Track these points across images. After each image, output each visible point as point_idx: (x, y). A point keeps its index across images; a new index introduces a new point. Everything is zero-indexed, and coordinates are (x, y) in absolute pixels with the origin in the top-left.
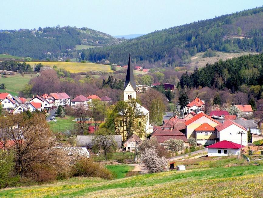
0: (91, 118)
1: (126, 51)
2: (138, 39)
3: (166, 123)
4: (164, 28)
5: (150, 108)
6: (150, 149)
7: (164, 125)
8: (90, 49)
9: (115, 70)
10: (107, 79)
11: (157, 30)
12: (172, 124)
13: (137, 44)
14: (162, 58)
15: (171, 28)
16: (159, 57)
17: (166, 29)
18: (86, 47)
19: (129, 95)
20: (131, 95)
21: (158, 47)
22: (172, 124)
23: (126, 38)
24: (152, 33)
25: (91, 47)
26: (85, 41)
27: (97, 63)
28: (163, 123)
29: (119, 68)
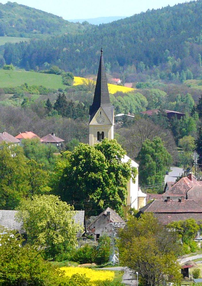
0: (76, 170)
1: (91, 47)
2: (115, 24)
3: (170, 187)
4: (165, 5)
5: (141, 158)
6: (142, 238)
7: (167, 191)
8: (197, 159)
9: (69, 85)
10: (53, 102)
11: (151, 9)
12: (184, 191)
13: (113, 34)
14: (161, 62)
15: (179, 5)
16: (154, 59)
17: (169, 6)
18: (15, 40)
19: (98, 133)
20: (103, 133)
21: (153, 39)
22: (184, 191)
23: (91, 22)
24: (142, 14)
25: (23, 40)
26: (13, 28)
27: (35, 70)
28: (165, 188)
29: (78, 81)
